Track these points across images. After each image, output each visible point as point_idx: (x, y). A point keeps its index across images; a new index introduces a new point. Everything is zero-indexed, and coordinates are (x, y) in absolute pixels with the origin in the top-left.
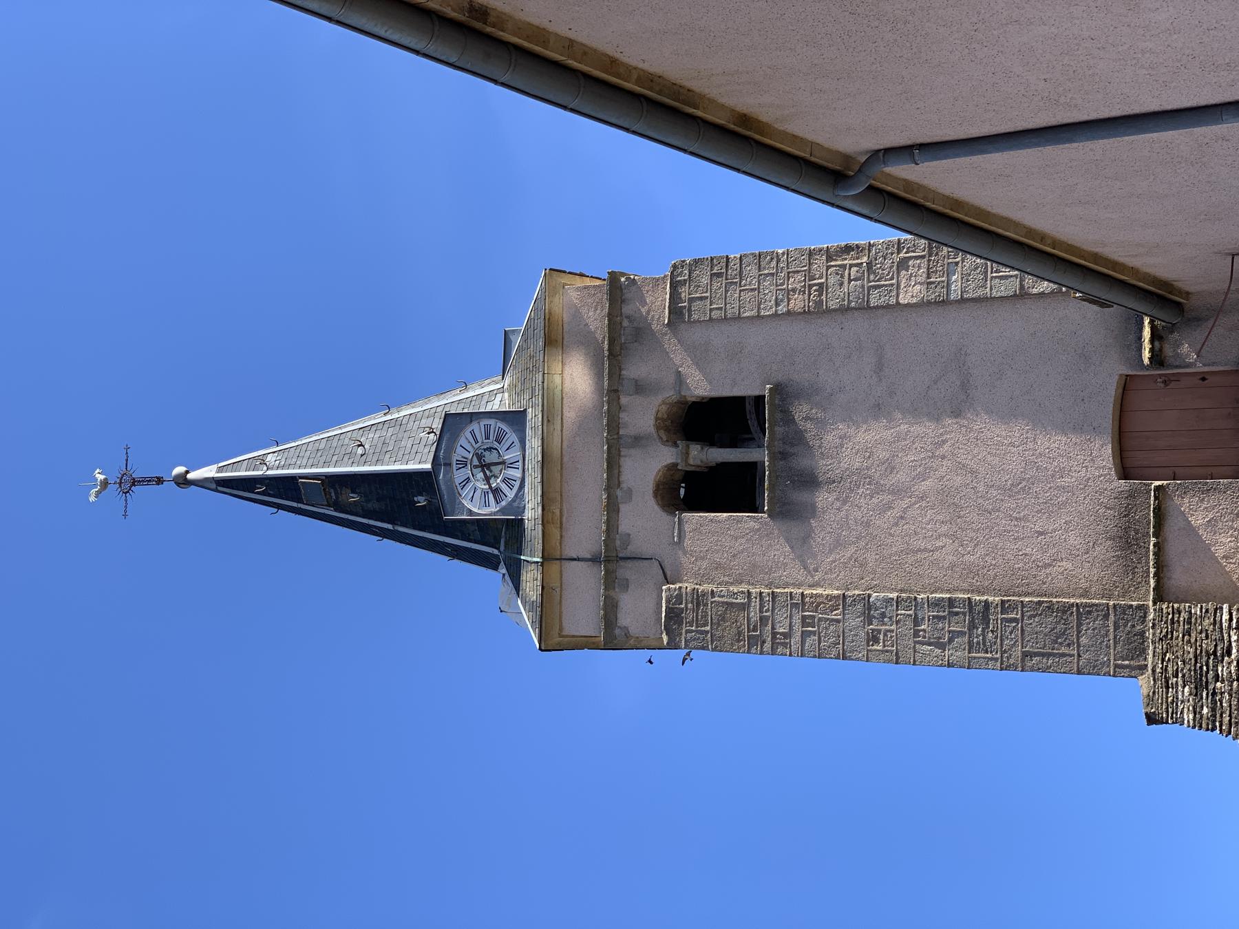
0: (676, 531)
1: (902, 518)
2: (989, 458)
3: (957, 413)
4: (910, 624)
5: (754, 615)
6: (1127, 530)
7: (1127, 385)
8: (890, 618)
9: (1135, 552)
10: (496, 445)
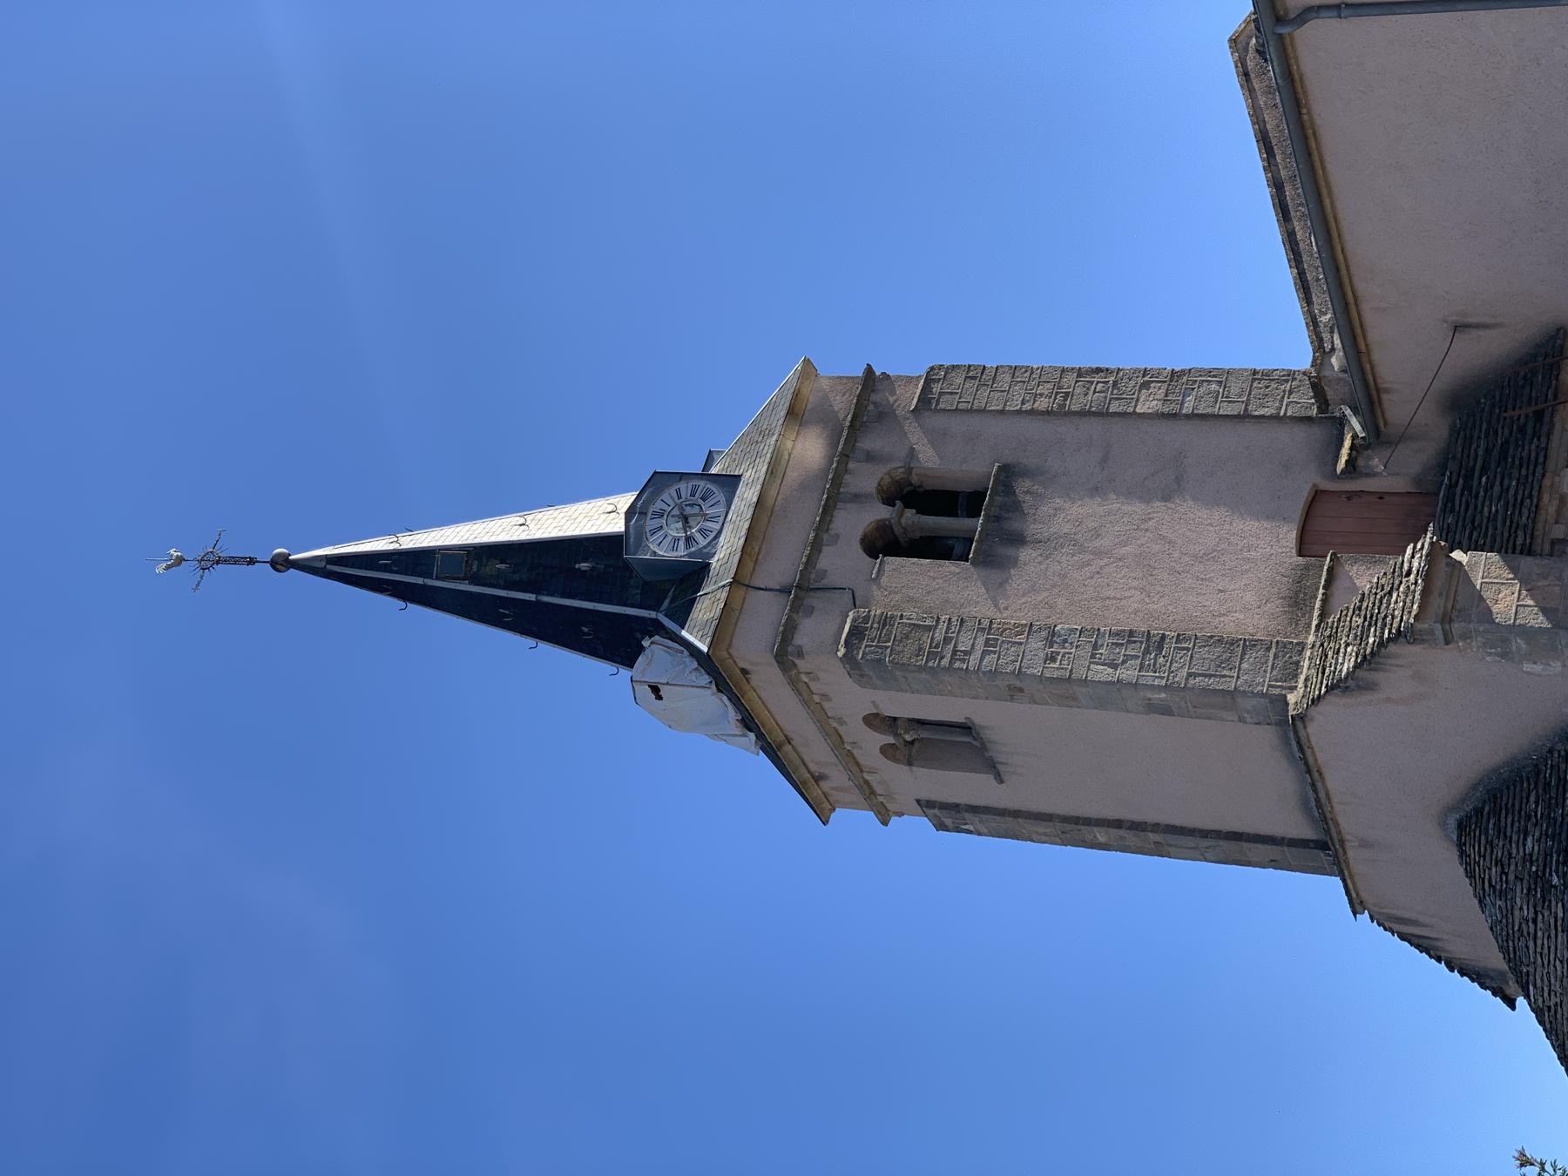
0: (876, 570)
1: (1098, 573)
2: (1188, 533)
3: (1166, 498)
4: (1089, 648)
5: (939, 635)
6: (1297, 593)
7: (1317, 495)
8: (1071, 643)
9: (1302, 609)
10: (700, 502)
